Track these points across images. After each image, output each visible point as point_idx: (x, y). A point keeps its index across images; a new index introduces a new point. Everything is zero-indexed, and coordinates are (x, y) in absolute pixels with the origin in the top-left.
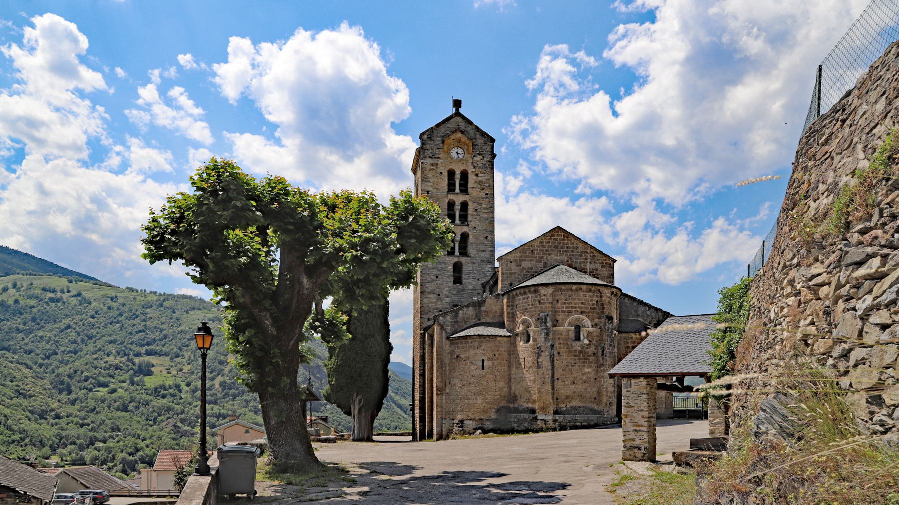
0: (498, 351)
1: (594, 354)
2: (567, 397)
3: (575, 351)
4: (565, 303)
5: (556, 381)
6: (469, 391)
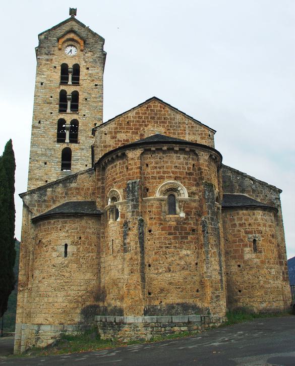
0: (84, 233)
1: (193, 230)
2: (162, 290)
3: (170, 227)
4: (156, 167)
5: (147, 267)
6: (49, 285)
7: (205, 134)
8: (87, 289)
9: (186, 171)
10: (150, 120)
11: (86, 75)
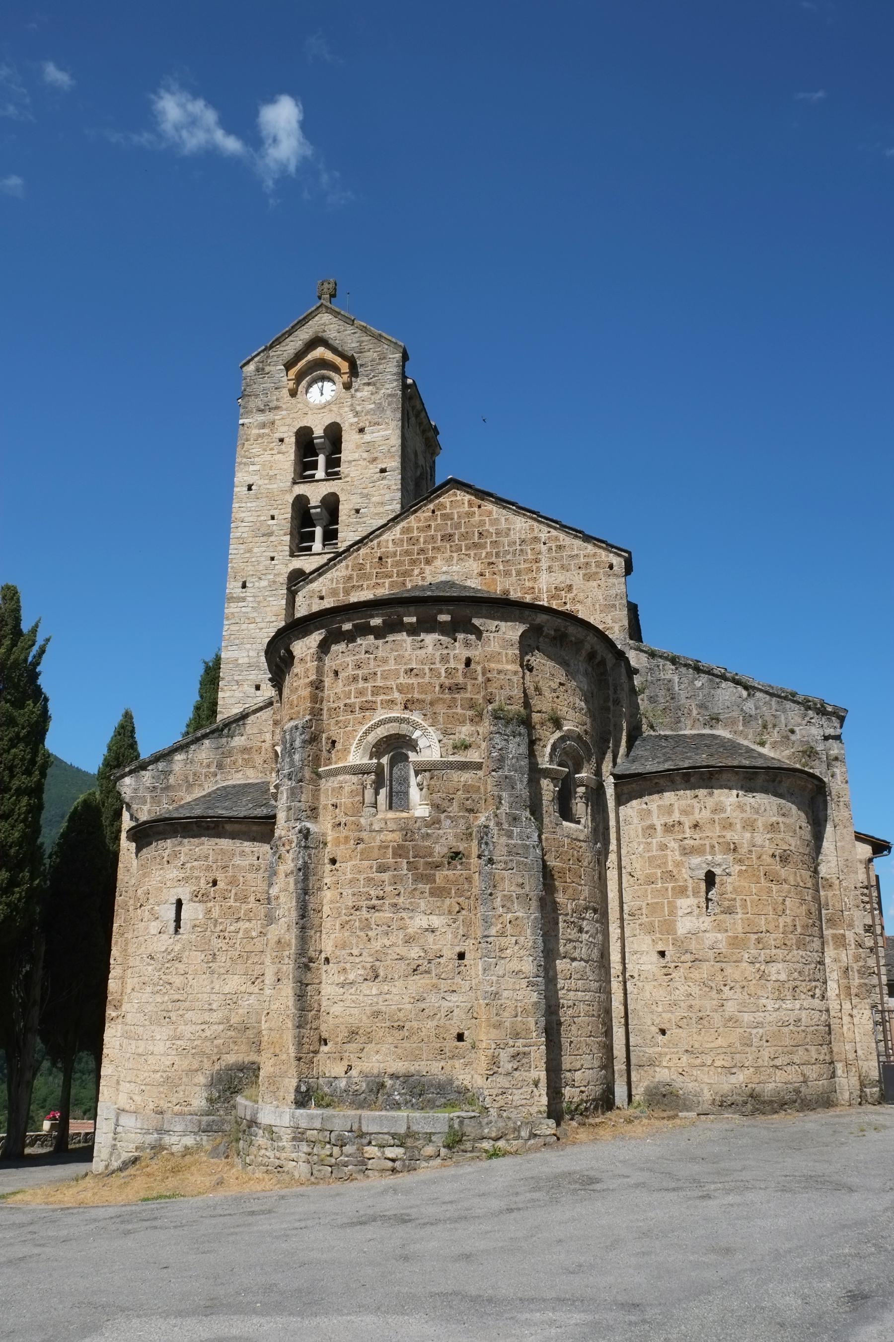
2: (353, 1033)
4: (355, 679)
7: (598, 564)
8: (228, 1021)
10: (439, 543)
11: (358, 447)
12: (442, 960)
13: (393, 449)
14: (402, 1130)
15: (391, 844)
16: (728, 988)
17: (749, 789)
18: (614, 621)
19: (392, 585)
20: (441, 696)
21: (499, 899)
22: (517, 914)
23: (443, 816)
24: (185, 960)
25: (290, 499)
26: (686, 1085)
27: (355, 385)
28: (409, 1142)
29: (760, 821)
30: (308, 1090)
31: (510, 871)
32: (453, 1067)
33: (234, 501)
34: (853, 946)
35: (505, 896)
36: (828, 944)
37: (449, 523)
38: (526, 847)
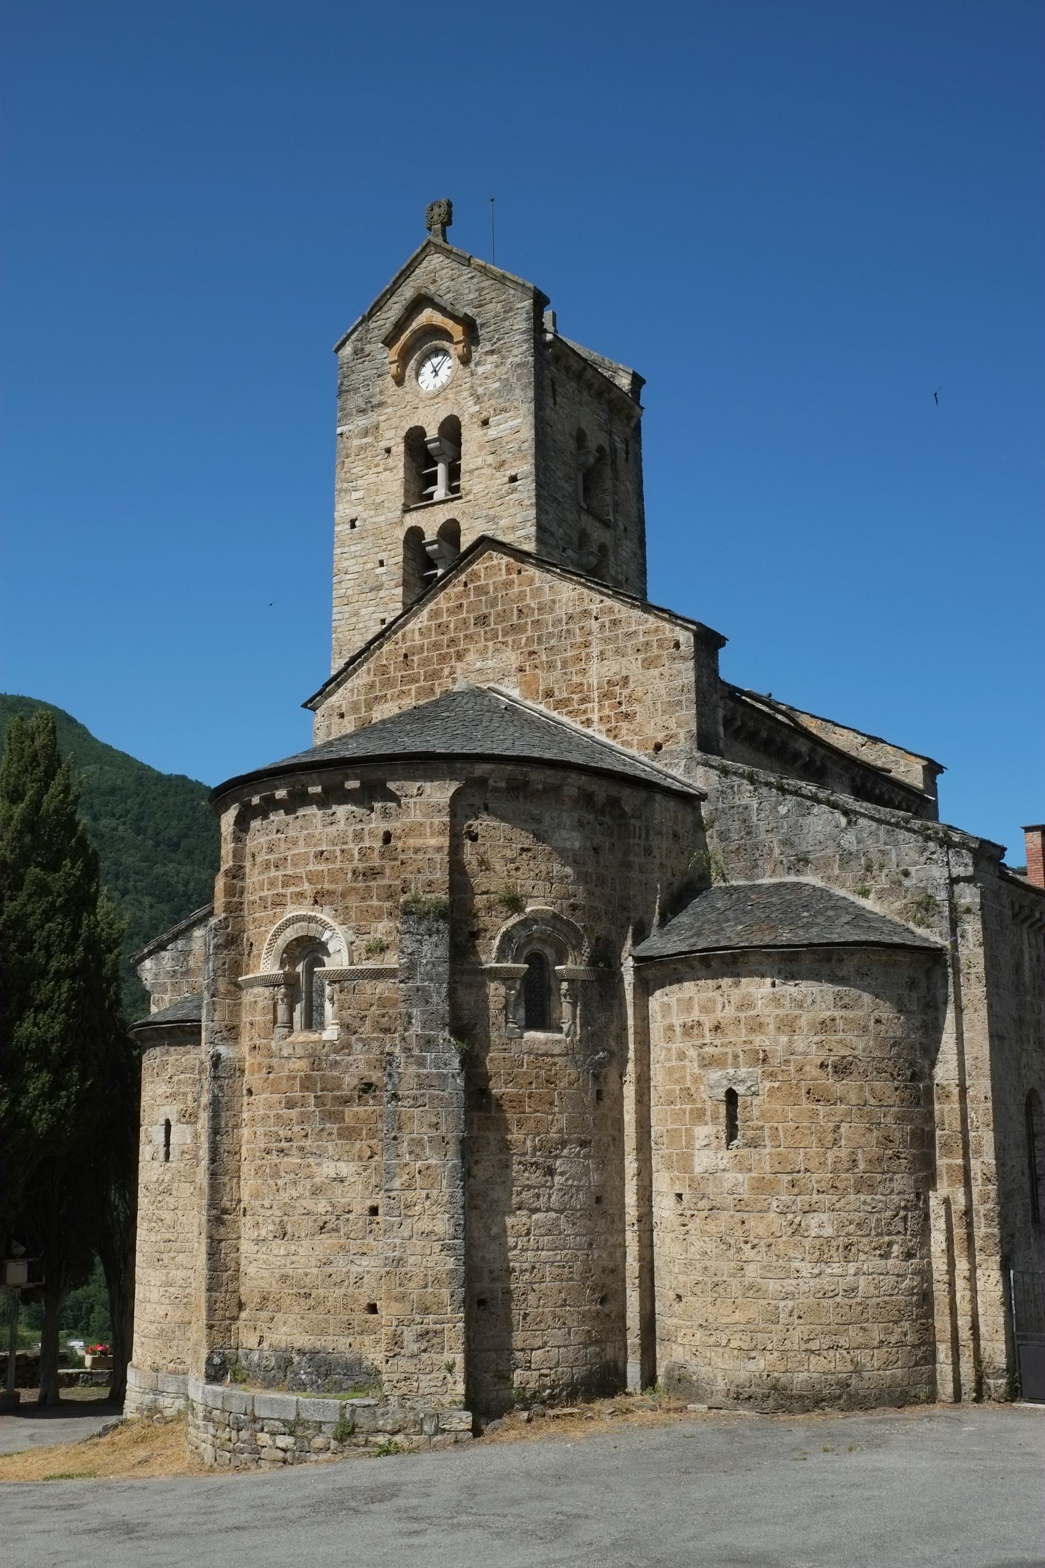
9: (356, 863)
11: (481, 448)
12: (351, 1216)
13: (526, 445)
14: (292, 1417)
15: (300, 1074)
16: (749, 1246)
17: (790, 976)
18: (679, 726)
19: (419, 694)
20: (353, 885)
21: (405, 1144)
22: (429, 1161)
23: (354, 1038)
24: (174, 1192)
25: (400, 534)
26: (700, 1370)
27: (476, 356)
28: (299, 1431)
29: (803, 1019)
30: (223, 1363)
31: (421, 1109)
32: (362, 1344)
33: (336, 545)
34: (980, 1181)
35: (413, 1140)
36: (942, 1179)
37: (483, 598)
38: (443, 1077)
